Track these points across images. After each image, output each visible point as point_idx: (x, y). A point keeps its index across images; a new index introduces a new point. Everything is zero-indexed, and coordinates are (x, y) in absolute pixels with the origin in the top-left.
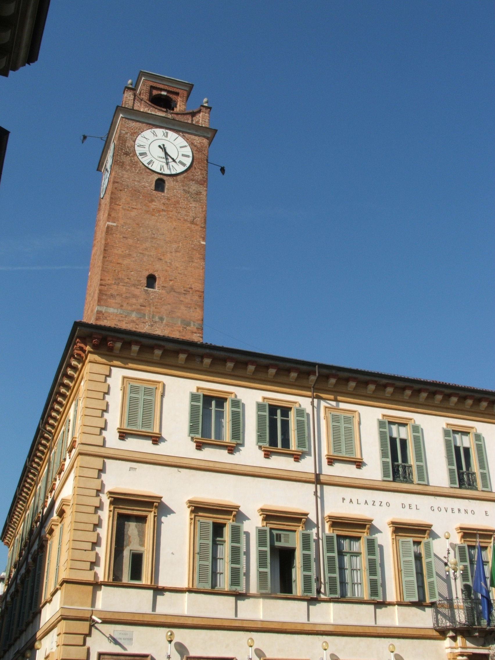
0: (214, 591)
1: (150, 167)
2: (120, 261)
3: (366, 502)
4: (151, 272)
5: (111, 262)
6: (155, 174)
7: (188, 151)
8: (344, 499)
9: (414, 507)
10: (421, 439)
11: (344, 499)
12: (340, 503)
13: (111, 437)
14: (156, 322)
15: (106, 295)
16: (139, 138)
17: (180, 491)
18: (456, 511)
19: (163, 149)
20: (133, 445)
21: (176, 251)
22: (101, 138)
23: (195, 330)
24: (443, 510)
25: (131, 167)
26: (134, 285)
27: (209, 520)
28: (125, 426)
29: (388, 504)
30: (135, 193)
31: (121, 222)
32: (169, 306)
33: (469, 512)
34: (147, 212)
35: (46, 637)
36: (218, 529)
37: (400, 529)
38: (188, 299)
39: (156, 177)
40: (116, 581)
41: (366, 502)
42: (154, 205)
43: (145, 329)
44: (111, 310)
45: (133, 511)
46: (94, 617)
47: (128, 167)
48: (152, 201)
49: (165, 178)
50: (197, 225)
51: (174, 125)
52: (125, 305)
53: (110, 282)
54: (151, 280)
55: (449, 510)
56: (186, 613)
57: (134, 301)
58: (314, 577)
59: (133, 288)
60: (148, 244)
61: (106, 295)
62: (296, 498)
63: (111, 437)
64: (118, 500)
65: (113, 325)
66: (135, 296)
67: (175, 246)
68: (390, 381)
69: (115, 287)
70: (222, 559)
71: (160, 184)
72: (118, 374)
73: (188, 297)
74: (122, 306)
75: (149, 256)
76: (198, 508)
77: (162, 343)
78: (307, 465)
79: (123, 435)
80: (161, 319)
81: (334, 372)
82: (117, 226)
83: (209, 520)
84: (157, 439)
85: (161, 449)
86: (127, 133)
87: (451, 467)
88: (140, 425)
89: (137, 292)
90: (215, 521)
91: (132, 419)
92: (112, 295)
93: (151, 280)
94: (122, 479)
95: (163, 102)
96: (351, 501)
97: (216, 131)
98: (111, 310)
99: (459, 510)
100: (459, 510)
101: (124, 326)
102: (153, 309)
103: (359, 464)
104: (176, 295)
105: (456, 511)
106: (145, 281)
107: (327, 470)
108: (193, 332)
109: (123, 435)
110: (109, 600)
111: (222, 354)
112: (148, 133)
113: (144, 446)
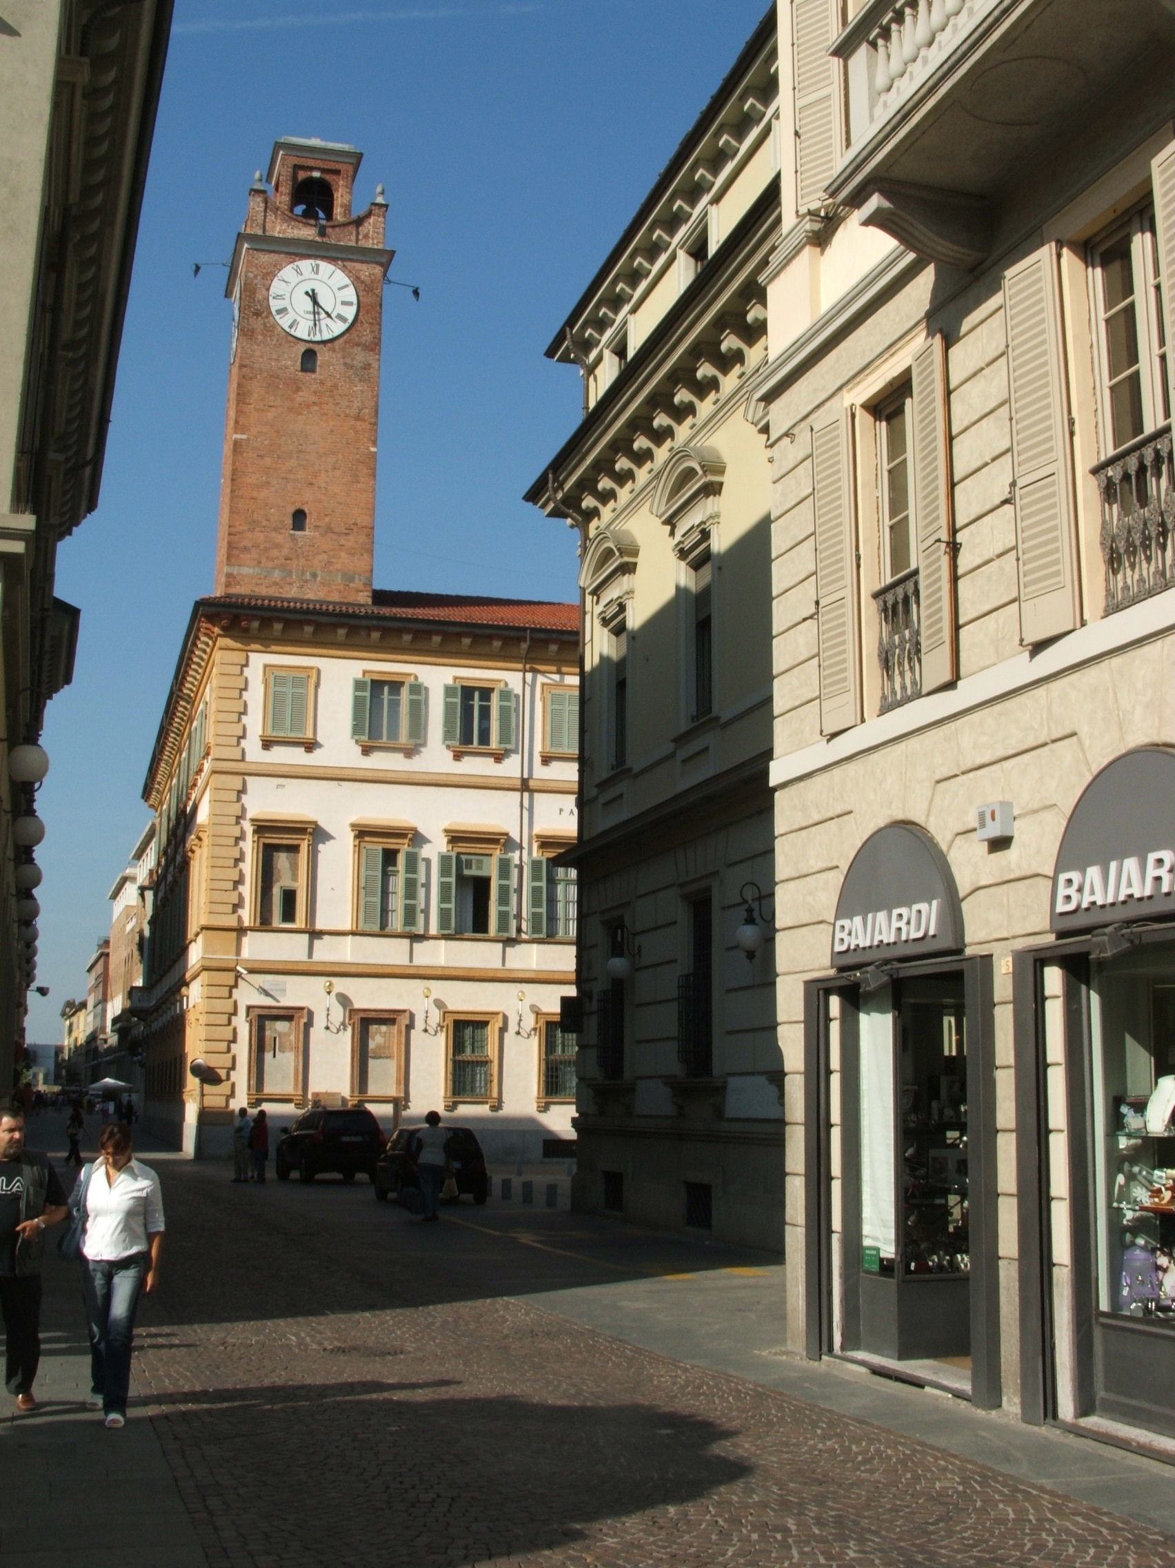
2: (255, 494)
7: (350, 294)
8: (561, 810)
11: (561, 810)
13: (252, 746)
17: (339, 811)
25: (265, 336)
26: (275, 530)
27: (376, 846)
34: (290, 409)
36: (390, 857)
39: (302, 348)
40: (264, 924)
42: (304, 396)
44: (246, 570)
45: (282, 841)
47: (260, 337)
48: (298, 389)
50: (364, 421)
52: (264, 560)
54: (299, 518)
57: (275, 553)
59: (273, 534)
60: (292, 463)
63: (252, 746)
64: (262, 828)
66: (278, 546)
67: (331, 460)
69: (250, 535)
71: (309, 358)
74: (260, 562)
76: (363, 832)
79: (267, 744)
82: (248, 439)
84: (311, 746)
88: (292, 728)
89: (279, 538)
90: (387, 848)
93: (299, 518)
94: (269, 801)
109: (267, 744)
110: (256, 947)
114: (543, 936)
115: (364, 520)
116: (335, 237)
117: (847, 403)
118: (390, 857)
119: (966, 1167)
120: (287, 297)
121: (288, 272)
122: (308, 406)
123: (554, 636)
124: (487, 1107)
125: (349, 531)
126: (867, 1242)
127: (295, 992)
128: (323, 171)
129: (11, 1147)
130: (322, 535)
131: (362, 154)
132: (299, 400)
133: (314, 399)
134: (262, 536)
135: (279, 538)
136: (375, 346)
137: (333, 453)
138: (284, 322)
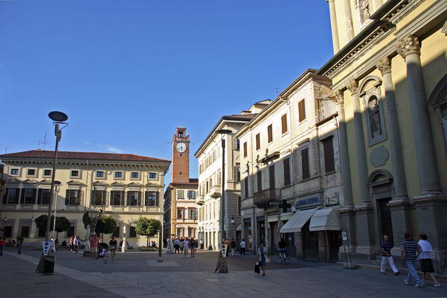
0: (191, 219)
10: (303, 149)
13: (177, 199)
17: (186, 226)
20: (180, 200)
27: (190, 210)
35: (347, 129)
36: (192, 211)
40: (178, 218)
45: (180, 210)
54: (181, 173)
63: (177, 199)
64: (178, 208)
70: (84, 256)
71: (181, 155)
72: (177, 189)
76: (189, 208)
79: (178, 199)
83: (190, 210)
84: (183, 199)
85: (184, 200)
88: (181, 197)
93: (181, 173)
94: (179, 205)
109: (178, 199)
110: (178, 221)
113: (181, 200)
115: (187, 172)
116: (185, 221)
117: (287, 137)
118: (192, 211)
119: (66, 202)
121: (178, 144)
124: (187, 236)
127: (184, 226)
129: (105, 220)
136: (189, 152)
138: (178, 150)
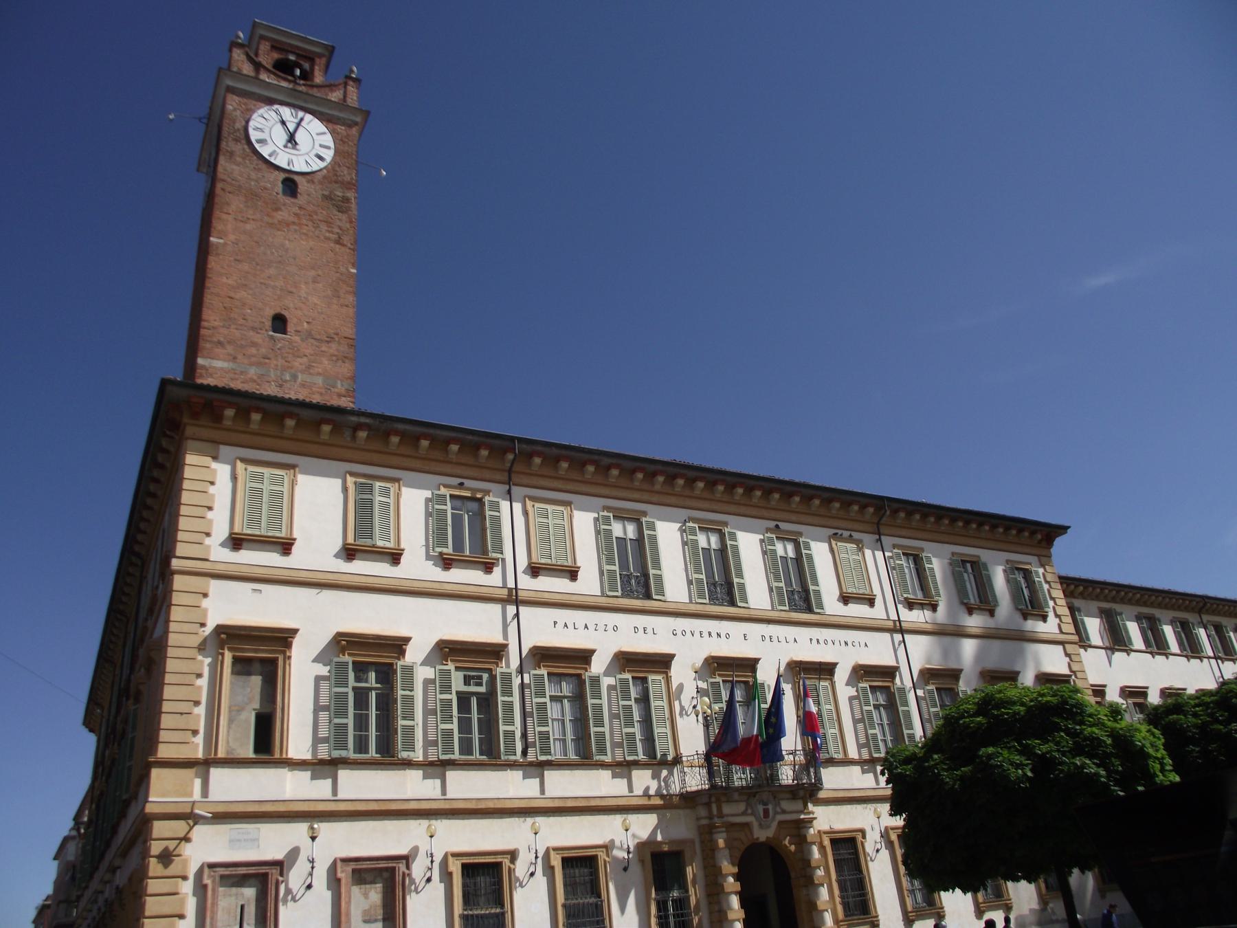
1: (272, 160)
2: (232, 294)
3: (586, 627)
4: (278, 310)
5: (218, 295)
6: (277, 173)
7: (328, 139)
8: (555, 623)
9: (649, 630)
11: (555, 623)
12: (543, 629)
14: (286, 381)
15: (211, 342)
16: (255, 116)
17: (314, 620)
18: (705, 634)
19: (291, 139)
21: (314, 282)
22: (200, 119)
23: (343, 391)
24: (830, 643)
25: (244, 158)
26: (253, 329)
28: (350, 540)
29: (615, 628)
30: (252, 196)
31: (232, 237)
32: (305, 359)
33: (723, 635)
34: (271, 225)
37: (625, 660)
38: (333, 348)
39: (282, 176)
41: (586, 627)
42: (282, 215)
43: (271, 390)
44: (218, 364)
46: (197, 811)
47: (239, 159)
48: (277, 209)
49: (296, 178)
50: (343, 245)
51: (305, 101)
52: (240, 357)
53: (216, 323)
55: (697, 634)
56: (288, 796)
57: (254, 351)
58: (518, 734)
59: (251, 333)
60: (272, 271)
61: (211, 342)
62: (478, 624)
65: (220, 385)
66: (254, 344)
67: (313, 273)
68: (614, 461)
69: (225, 331)
73: (334, 346)
74: (235, 358)
75: (274, 287)
77: (296, 410)
78: (495, 578)
80: (295, 377)
81: (539, 448)
82: (225, 244)
84: (286, 547)
86: (235, 110)
87: (658, 572)
89: (258, 338)
90: (369, 661)
91: (254, 520)
92: (220, 343)
93: (280, 323)
95: (283, 68)
96: (566, 625)
97: (368, 113)
98: (218, 364)
99: (710, 634)
100: (710, 634)
101: (237, 385)
102: (280, 362)
103: (573, 574)
104: (315, 343)
105: (705, 634)
106: (268, 324)
107: (527, 583)
108: (340, 395)
109: (236, 542)
111: (555, 451)
112: (264, 111)
114: (619, 594)
120: (267, 131)
122: (288, 225)
123: (539, 448)
125: (330, 339)
126: (957, 890)
128: (298, 55)
130: (302, 340)
131: (333, 47)
132: (280, 218)
133: (291, 219)
134: (237, 333)
135: (258, 338)
137: (313, 268)
